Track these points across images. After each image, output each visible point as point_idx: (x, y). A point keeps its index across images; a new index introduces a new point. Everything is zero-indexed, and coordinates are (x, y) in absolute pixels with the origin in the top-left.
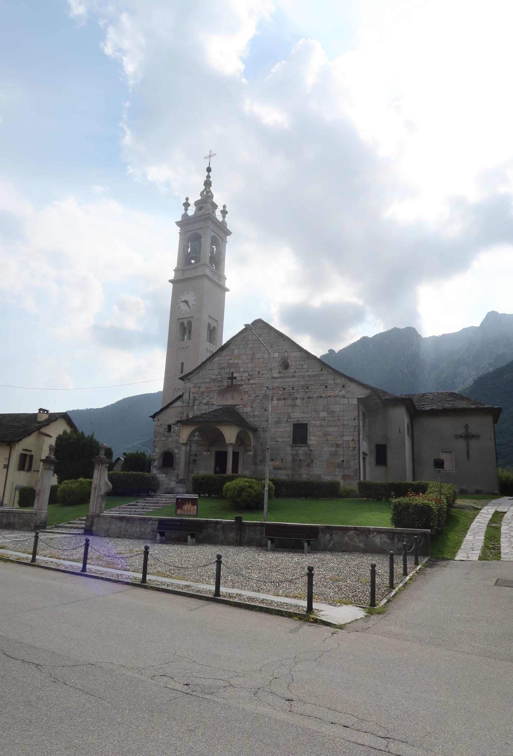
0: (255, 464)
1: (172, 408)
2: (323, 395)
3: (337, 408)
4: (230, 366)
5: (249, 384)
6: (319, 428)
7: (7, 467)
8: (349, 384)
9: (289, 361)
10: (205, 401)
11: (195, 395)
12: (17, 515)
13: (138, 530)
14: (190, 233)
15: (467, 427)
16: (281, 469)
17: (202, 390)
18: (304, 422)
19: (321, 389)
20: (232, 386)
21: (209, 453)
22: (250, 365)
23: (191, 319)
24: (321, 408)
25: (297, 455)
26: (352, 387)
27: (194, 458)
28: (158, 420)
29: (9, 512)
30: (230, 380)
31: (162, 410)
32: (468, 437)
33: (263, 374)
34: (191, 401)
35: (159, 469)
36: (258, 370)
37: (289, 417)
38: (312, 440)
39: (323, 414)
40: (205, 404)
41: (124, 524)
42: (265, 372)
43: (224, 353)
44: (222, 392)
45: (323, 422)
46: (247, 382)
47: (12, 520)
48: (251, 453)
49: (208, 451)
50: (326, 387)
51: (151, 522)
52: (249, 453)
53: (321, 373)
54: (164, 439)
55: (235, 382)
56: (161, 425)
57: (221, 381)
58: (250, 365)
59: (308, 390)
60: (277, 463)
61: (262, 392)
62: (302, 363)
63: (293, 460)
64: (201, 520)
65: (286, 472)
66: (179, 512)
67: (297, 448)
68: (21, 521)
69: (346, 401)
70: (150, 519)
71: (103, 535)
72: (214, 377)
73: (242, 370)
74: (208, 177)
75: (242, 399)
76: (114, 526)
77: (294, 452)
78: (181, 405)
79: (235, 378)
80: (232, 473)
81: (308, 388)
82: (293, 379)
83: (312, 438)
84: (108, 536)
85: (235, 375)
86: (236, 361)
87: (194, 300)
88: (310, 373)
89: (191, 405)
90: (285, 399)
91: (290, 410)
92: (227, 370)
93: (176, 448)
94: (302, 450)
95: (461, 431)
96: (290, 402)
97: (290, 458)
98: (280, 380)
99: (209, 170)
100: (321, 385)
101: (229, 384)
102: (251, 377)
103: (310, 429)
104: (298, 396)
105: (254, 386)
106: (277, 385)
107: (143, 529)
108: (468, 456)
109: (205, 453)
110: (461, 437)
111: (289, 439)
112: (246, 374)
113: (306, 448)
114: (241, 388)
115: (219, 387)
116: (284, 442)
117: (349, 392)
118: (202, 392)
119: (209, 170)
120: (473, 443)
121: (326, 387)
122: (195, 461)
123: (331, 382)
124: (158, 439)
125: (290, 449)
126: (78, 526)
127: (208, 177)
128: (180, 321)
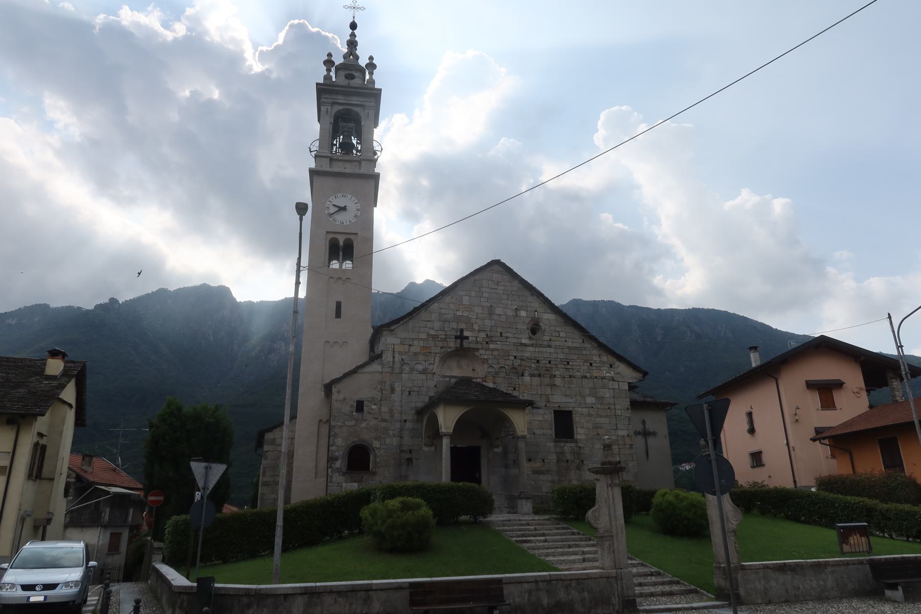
0: (506, 466)
1: (364, 373)
2: (588, 375)
3: (607, 394)
4: (458, 319)
5: (488, 349)
6: (587, 418)
7: (8, 472)
8: (617, 363)
9: (541, 324)
10: (420, 367)
11: (403, 357)
12: (574, 584)
13: (814, 584)
14: (341, 107)
15: (644, 422)
16: (542, 473)
17: (413, 349)
18: (568, 409)
19: (585, 367)
20: (462, 350)
21: (433, 448)
22: (488, 323)
23: (351, 237)
24: (587, 391)
25: (562, 453)
26: (622, 368)
27: (408, 456)
28: (339, 392)
29: (551, 581)
30: (459, 341)
31: (346, 376)
32: (646, 434)
33: (507, 338)
34: (397, 365)
35: (344, 474)
36: (499, 330)
37: (548, 401)
38: (580, 433)
39: (590, 400)
40: (420, 373)
41: (788, 577)
42: (509, 335)
43: (447, 299)
44: (447, 357)
45: (591, 410)
46: (485, 346)
47: (562, 595)
48: (499, 450)
49: (432, 445)
50: (591, 364)
51: (829, 569)
52: (496, 450)
53: (582, 345)
54: (353, 423)
55: (466, 344)
56: (345, 399)
57: (445, 340)
58: (488, 323)
59: (569, 367)
60: (537, 465)
61: (508, 363)
62: (558, 329)
63: (558, 461)
64: (880, 559)
65: (550, 478)
66: (846, 548)
67: (562, 444)
68: (586, 594)
69: (616, 385)
70: (826, 564)
71: (759, 601)
72: (432, 332)
73: (476, 327)
74: (353, 35)
75: (474, 370)
76: (773, 584)
77: (559, 450)
78: (380, 370)
79: (467, 338)
80: (455, 476)
81: (568, 363)
82: (549, 350)
83: (580, 430)
84: (769, 603)
85: (466, 334)
86: (466, 314)
87: (358, 210)
88: (570, 344)
89: (397, 371)
90: (539, 375)
91: (548, 391)
92: (454, 325)
93: (376, 439)
94: (568, 447)
95: (640, 428)
96: (547, 380)
97: (554, 457)
98: (531, 349)
99: (353, 26)
100: (586, 361)
101: (458, 345)
102: (489, 340)
103: (576, 418)
104: (557, 373)
105: (496, 353)
106: (528, 355)
107: (821, 583)
108: (647, 455)
109: (425, 449)
110: (639, 433)
111: (550, 432)
112: (483, 335)
113: (573, 445)
114: (477, 353)
115: (442, 348)
116: (544, 435)
117: (618, 373)
118: (416, 354)
119: (353, 26)
120: (651, 441)
121: (591, 364)
122: (409, 460)
123: (596, 359)
124: (340, 424)
125: (552, 445)
126: (652, 589)
127: (353, 35)
128: (331, 236)
